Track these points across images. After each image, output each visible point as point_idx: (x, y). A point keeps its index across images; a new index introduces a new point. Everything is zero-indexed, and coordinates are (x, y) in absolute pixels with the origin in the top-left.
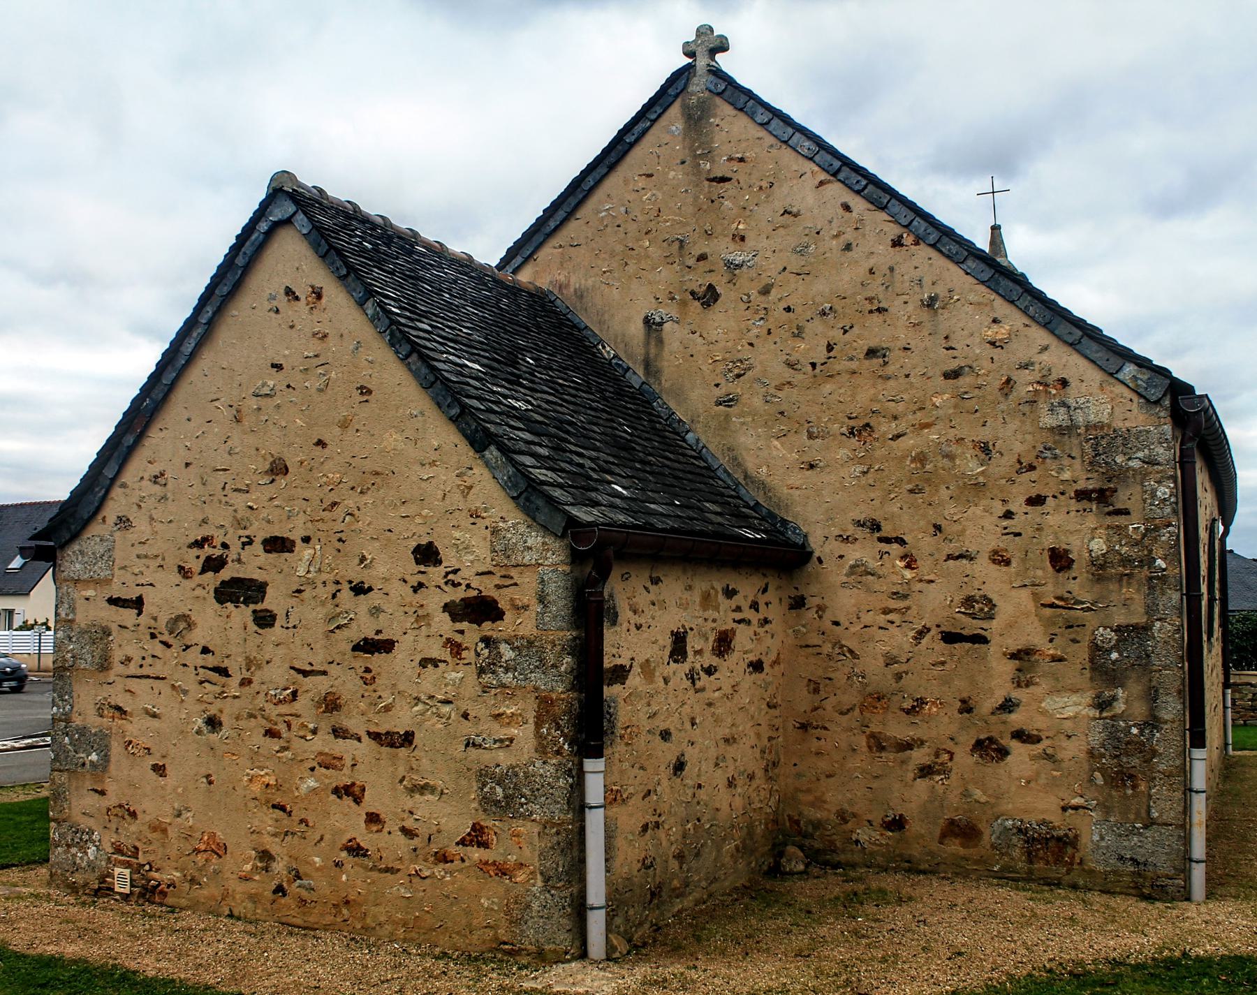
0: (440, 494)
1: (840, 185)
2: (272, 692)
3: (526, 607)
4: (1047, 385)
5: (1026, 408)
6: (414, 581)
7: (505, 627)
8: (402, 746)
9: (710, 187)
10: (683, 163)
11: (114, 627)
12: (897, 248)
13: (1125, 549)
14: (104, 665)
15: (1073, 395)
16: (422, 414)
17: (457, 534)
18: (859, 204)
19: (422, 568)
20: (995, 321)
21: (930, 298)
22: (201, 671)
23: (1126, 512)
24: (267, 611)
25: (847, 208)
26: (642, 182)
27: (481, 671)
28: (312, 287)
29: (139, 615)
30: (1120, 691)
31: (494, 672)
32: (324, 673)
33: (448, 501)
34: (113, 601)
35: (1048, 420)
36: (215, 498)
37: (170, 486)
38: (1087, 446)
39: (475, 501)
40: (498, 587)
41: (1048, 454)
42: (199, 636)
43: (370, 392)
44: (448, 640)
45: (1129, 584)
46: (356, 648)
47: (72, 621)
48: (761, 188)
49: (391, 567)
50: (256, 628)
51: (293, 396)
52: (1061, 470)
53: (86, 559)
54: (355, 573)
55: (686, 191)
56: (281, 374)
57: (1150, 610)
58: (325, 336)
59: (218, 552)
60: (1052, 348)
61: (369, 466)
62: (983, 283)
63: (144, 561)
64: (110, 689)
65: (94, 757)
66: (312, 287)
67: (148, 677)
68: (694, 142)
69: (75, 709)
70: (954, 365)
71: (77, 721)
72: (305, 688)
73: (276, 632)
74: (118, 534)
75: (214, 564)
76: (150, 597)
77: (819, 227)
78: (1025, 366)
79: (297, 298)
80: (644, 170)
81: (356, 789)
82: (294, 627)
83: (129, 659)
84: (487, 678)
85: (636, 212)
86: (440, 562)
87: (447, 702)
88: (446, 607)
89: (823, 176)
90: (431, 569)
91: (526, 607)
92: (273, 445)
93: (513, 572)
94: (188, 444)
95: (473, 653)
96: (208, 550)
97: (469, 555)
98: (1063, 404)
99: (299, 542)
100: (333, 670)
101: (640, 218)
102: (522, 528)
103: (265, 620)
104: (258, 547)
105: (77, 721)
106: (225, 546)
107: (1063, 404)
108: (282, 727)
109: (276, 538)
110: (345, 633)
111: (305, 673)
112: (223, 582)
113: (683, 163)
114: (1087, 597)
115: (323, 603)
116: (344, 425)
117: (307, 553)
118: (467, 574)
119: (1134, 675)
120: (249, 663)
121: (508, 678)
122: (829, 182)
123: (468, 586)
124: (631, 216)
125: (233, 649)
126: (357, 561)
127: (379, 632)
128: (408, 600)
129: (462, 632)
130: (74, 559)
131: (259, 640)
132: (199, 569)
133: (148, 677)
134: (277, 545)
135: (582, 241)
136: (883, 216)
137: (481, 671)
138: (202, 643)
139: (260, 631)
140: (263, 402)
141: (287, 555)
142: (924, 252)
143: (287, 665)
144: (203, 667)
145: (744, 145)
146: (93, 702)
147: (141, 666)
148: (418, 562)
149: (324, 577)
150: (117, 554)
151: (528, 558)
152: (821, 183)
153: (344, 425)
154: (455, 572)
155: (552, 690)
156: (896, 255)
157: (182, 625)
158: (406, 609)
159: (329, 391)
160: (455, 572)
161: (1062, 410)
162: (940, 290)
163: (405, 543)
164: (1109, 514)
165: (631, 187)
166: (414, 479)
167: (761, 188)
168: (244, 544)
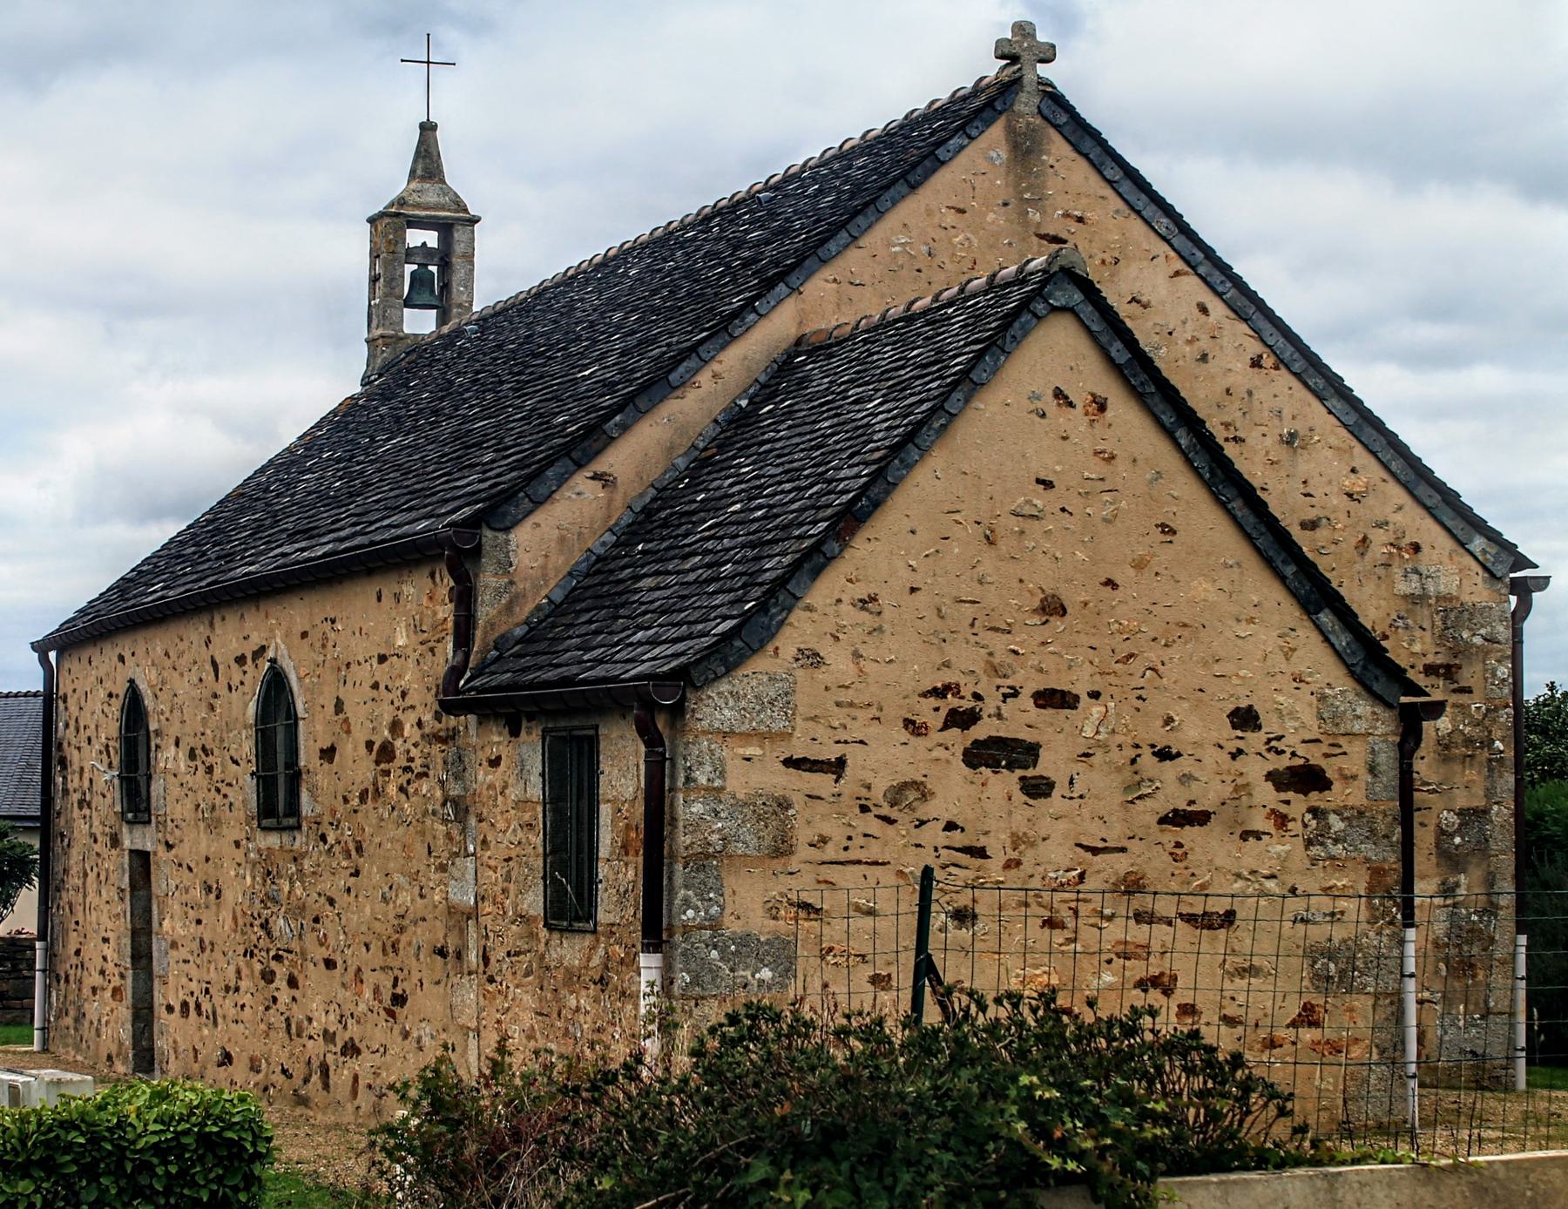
0: (1260, 654)
1: (1196, 280)
2: (1052, 875)
3: (1354, 777)
4: (1399, 549)
5: (1381, 571)
6: (1232, 746)
7: (1338, 795)
8: (1221, 926)
9: (1040, 246)
10: (1005, 204)
11: (798, 800)
12: (1256, 370)
13: (1468, 729)
14: (781, 849)
15: (1426, 560)
16: (1239, 564)
17: (1281, 699)
18: (1218, 309)
19: (1239, 733)
20: (1353, 471)
21: (1290, 434)
22: (943, 852)
23: (1469, 690)
24: (1042, 777)
25: (1204, 310)
26: (951, 218)
27: (1309, 843)
28: (1093, 395)
29: (836, 781)
30: (1462, 876)
31: (1322, 844)
32: (1123, 850)
33: (1269, 662)
34: (789, 763)
35: (1403, 587)
36: (959, 637)
37: (887, 614)
38: (1437, 618)
39: (1300, 664)
40: (1326, 756)
41: (1400, 623)
42: (939, 808)
43: (1173, 532)
44: (1273, 811)
45: (1471, 765)
46: (1163, 821)
47: (721, 789)
48: (1103, 262)
49: (1201, 731)
50: (1025, 798)
51: (1071, 523)
52: (1412, 642)
53: (743, 704)
54: (1161, 738)
55: (1010, 244)
56: (1050, 494)
57: (1489, 793)
58: (1113, 458)
59: (967, 704)
60: (1406, 508)
61: (1172, 616)
62: (1345, 426)
63: (846, 710)
64: (792, 882)
65: (766, 974)
66: (1093, 395)
67: (859, 862)
68: (1021, 178)
69: (728, 911)
70: (1311, 514)
71: (732, 927)
72: (1096, 868)
73: (1056, 802)
74: (800, 673)
75: (962, 719)
76: (854, 755)
77: (1171, 327)
78: (1380, 525)
79: (1071, 405)
80: (953, 202)
81: (1166, 979)
82: (1081, 797)
83: (824, 840)
84: (1316, 850)
85: (943, 257)
86: (1260, 728)
87: (1273, 876)
88: (1270, 776)
89: (1179, 265)
90: (1249, 735)
91: (1354, 777)
92: (1045, 578)
93: (1341, 741)
94: (913, 563)
95: (1300, 823)
96: (951, 701)
97: (1294, 723)
98: (1416, 571)
99: (1084, 698)
100: (1134, 846)
101: (948, 266)
102: (1351, 696)
103: (1038, 789)
104: (1025, 700)
105: (732, 927)
106: (977, 697)
107: (1416, 571)
108: (1065, 914)
109: (1054, 691)
110: (1148, 802)
111: (1095, 851)
112: (976, 742)
113: (1005, 204)
114: (1433, 778)
115: (1119, 770)
116: (1139, 565)
117: (1097, 710)
118: (1291, 741)
119: (1475, 860)
120: (1017, 841)
121: (1337, 850)
122: (1186, 274)
123: (1293, 754)
124: (937, 260)
125: (991, 824)
126: (1160, 722)
127: (1191, 803)
128: (1225, 767)
129: (1288, 802)
130: (721, 703)
131: (1029, 812)
132: (940, 725)
133: (859, 862)
134: (1052, 699)
135: (866, 279)
136: (1244, 328)
137: (1309, 843)
138: (947, 817)
139: (1031, 802)
140: (1029, 525)
141: (1067, 711)
142: (1284, 379)
143: (1072, 842)
144: (947, 847)
145: (1084, 201)
146: (760, 900)
147: (846, 849)
148: (1234, 727)
149: (1119, 739)
150: (799, 698)
151: (1358, 727)
152: (1177, 274)
153: (1139, 565)
154: (1279, 738)
155: (1385, 860)
156: (1254, 378)
157: (912, 795)
158: (1224, 777)
159: (1118, 523)
160: (1279, 738)
161: (1415, 577)
162: (1300, 426)
163: (1219, 705)
164: (1454, 691)
165: (936, 220)
166: (1229, 634)
167: (1103, 262)
168: (1005, 696)
